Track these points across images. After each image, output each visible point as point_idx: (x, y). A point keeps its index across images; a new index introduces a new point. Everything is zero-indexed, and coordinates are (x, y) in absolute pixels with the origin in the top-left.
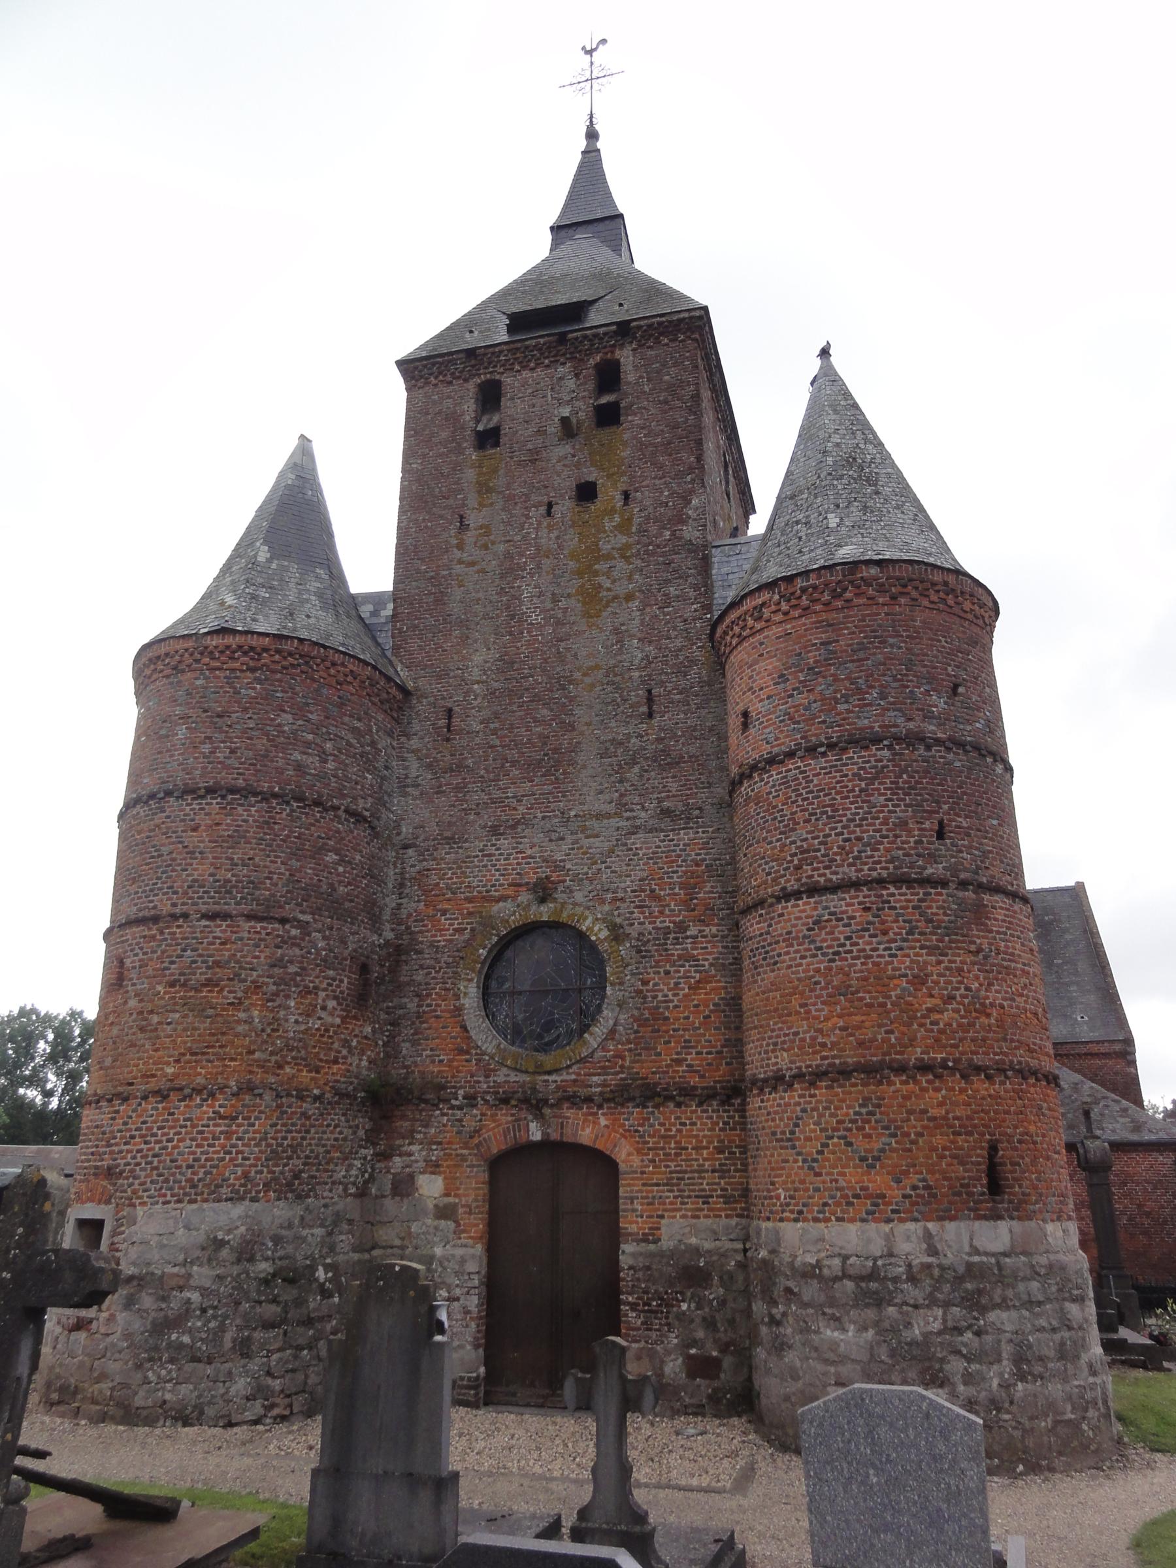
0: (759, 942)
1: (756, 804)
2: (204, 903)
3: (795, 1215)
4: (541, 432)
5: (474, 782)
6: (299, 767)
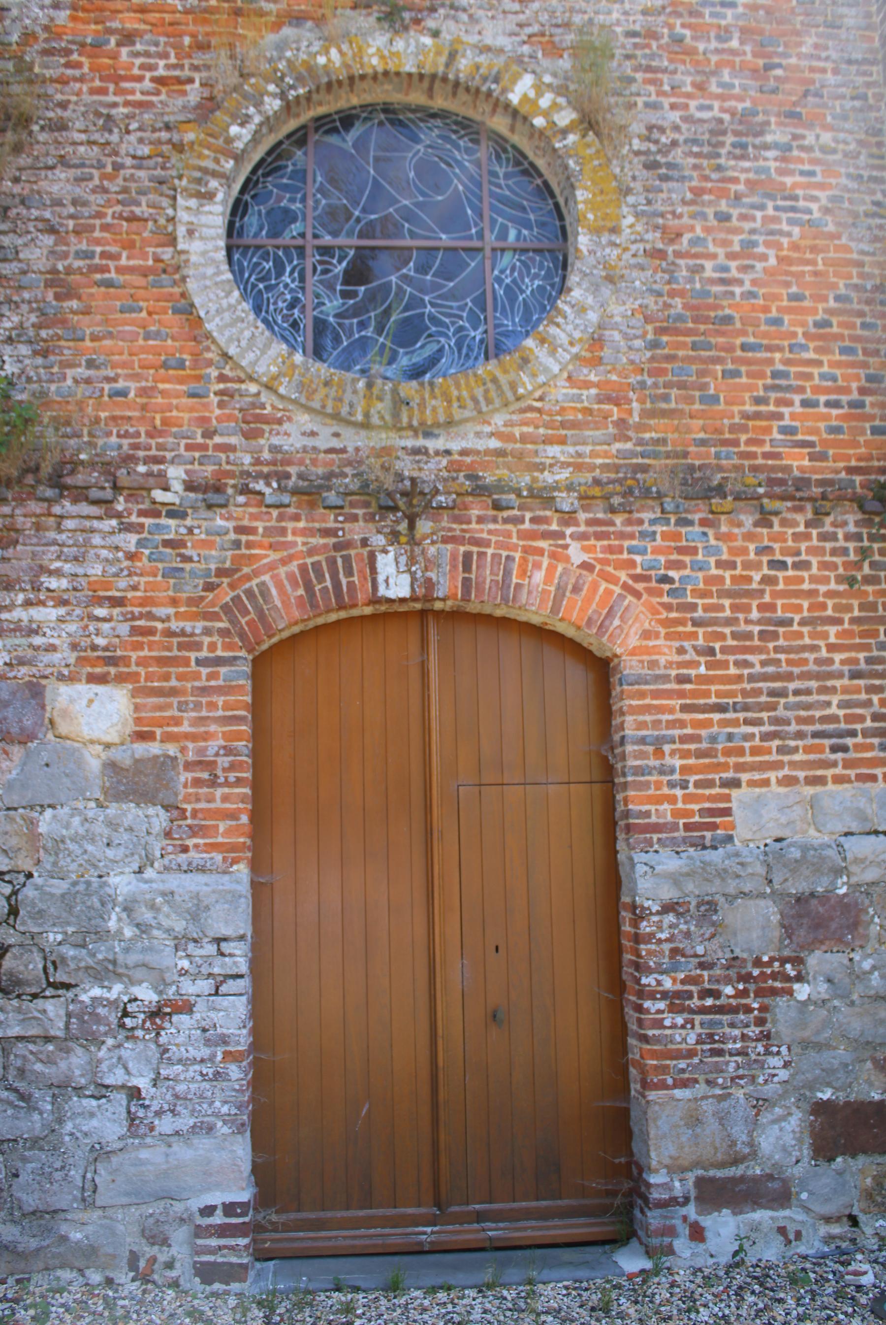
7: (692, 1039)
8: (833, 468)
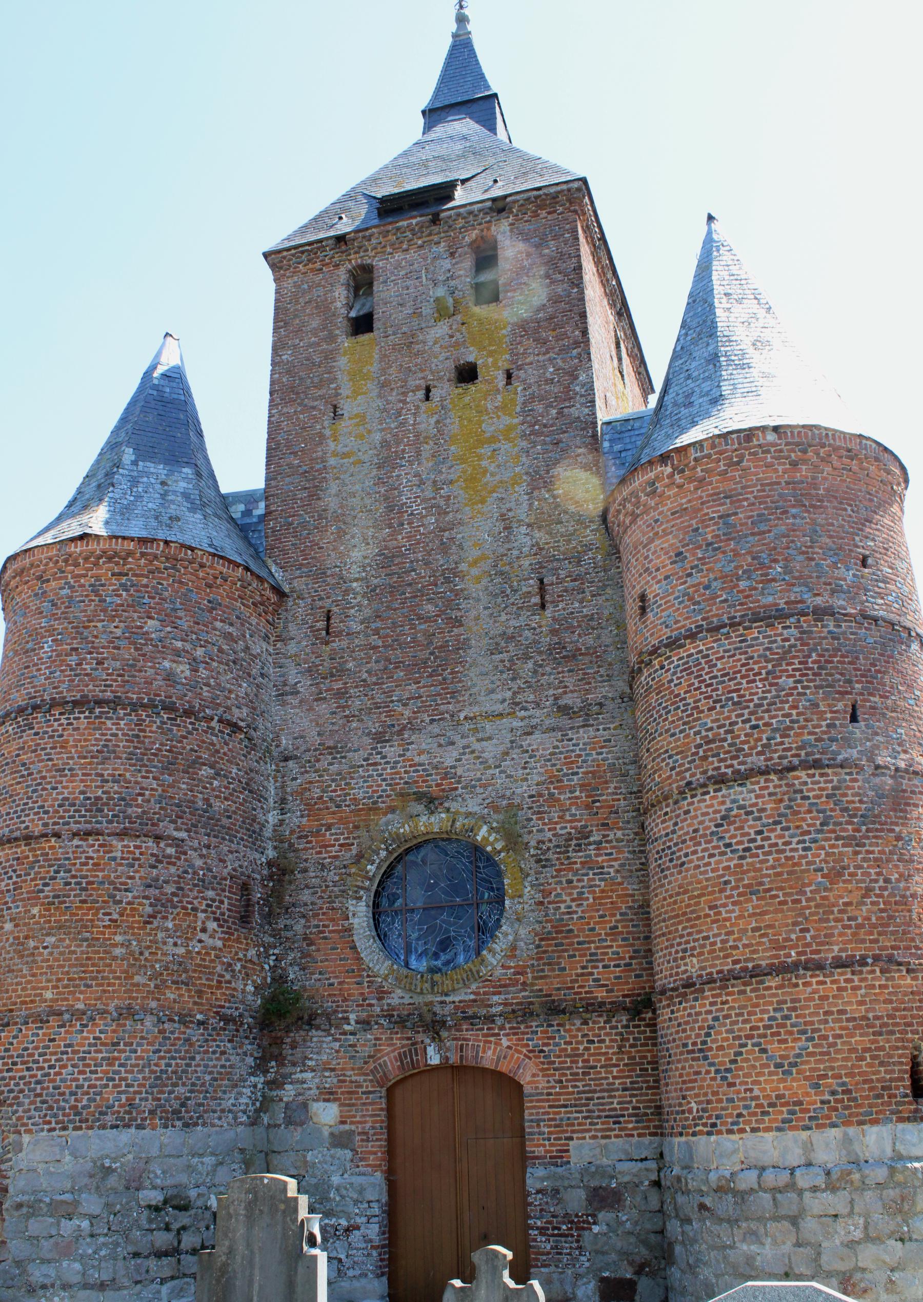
0: (664, 843)
1: (657, 694)
2: (76, 822)
4: (417, 314)
5: (356, 687)
6: (170, 677)
7: (548, 1247)
8: (617, 996)
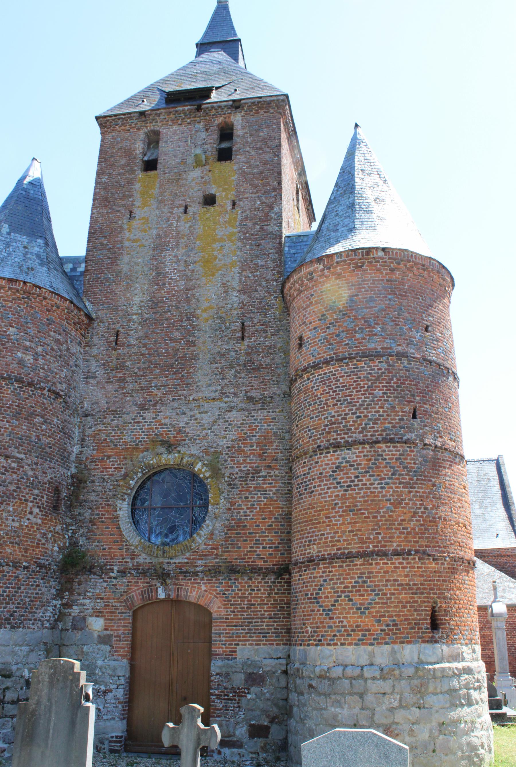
0: (303, 479)
1: (305, 394)
3: (317, 642)
5: (131, 377)
6: (21, 362)
